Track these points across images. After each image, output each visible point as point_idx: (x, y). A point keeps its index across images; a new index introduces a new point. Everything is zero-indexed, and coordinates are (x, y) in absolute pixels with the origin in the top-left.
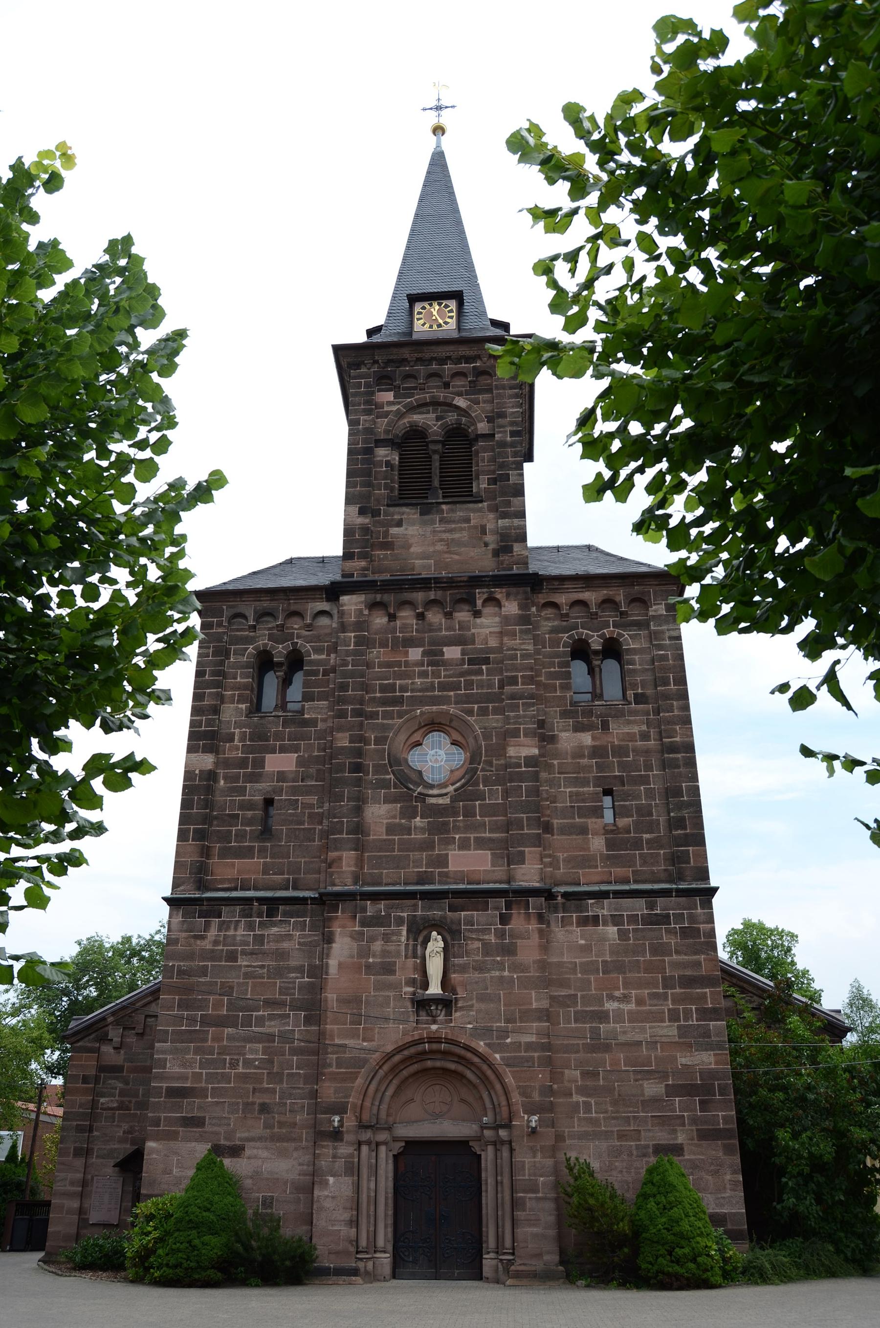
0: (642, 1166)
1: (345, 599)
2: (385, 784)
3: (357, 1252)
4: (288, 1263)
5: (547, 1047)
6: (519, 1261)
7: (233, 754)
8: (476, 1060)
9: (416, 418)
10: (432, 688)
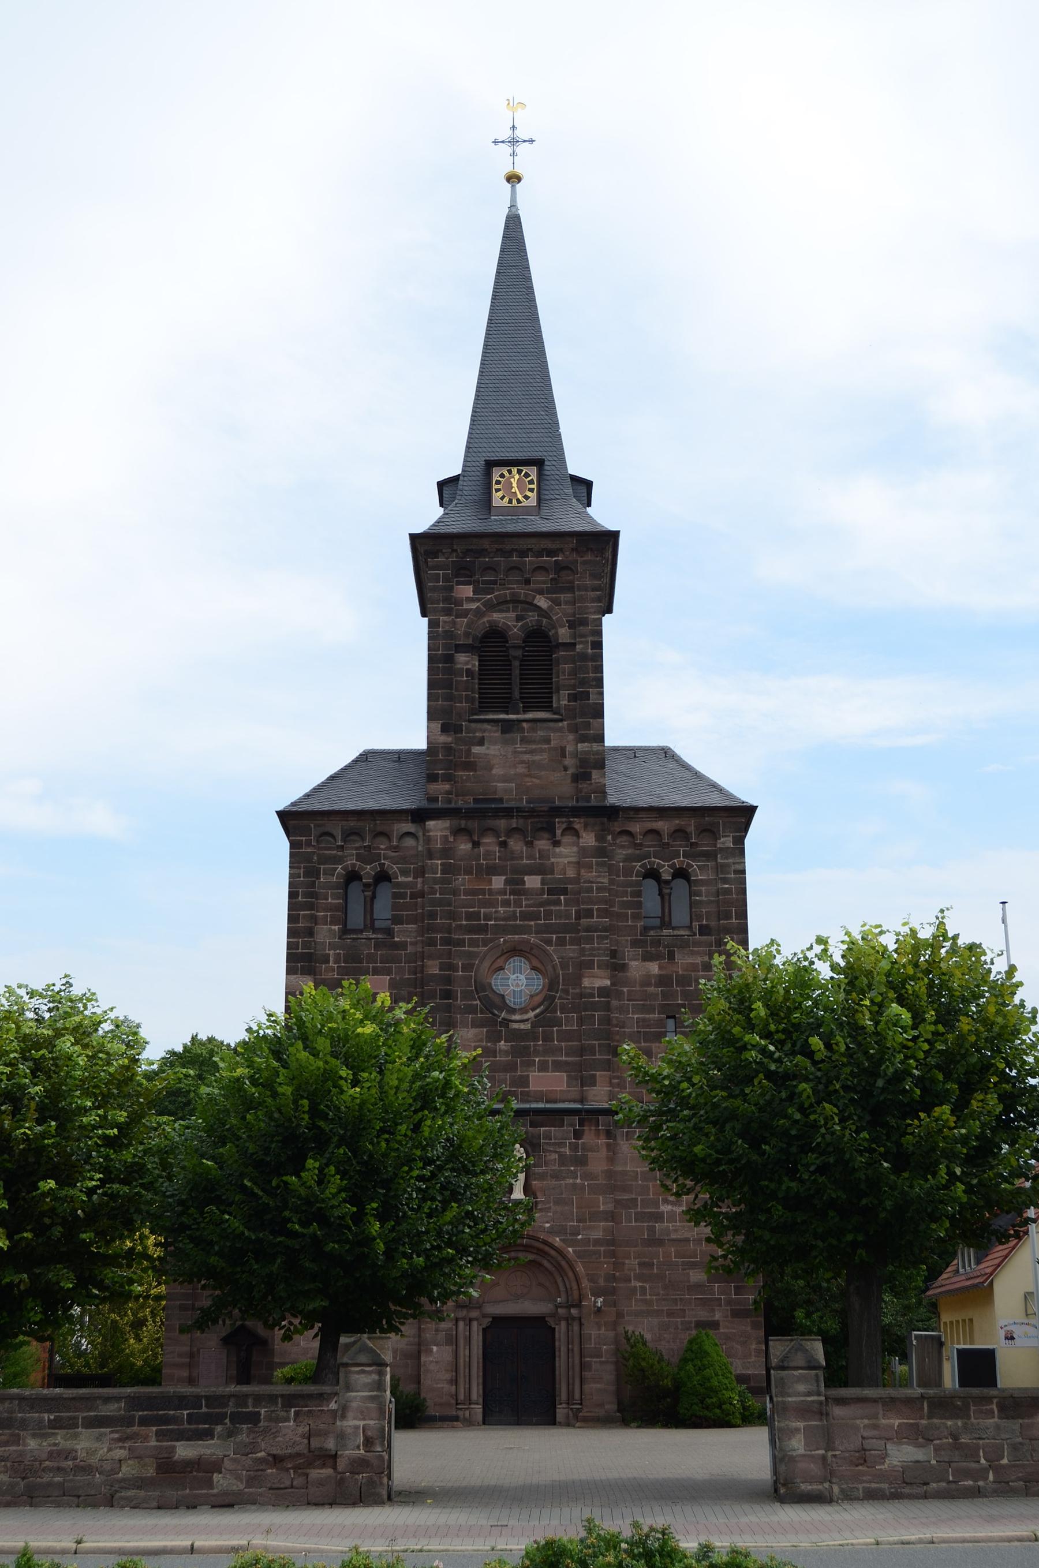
0: (686, 1337)
1: (431, 824)
2: (472, 1010)
3: (457, 1404)
4: (408, 1411)
5: (612, 1242)
6: (585, 1410)
7: (330, 975)
8: (553, 1253)
9: (496, 616)
10: (514, 917)
